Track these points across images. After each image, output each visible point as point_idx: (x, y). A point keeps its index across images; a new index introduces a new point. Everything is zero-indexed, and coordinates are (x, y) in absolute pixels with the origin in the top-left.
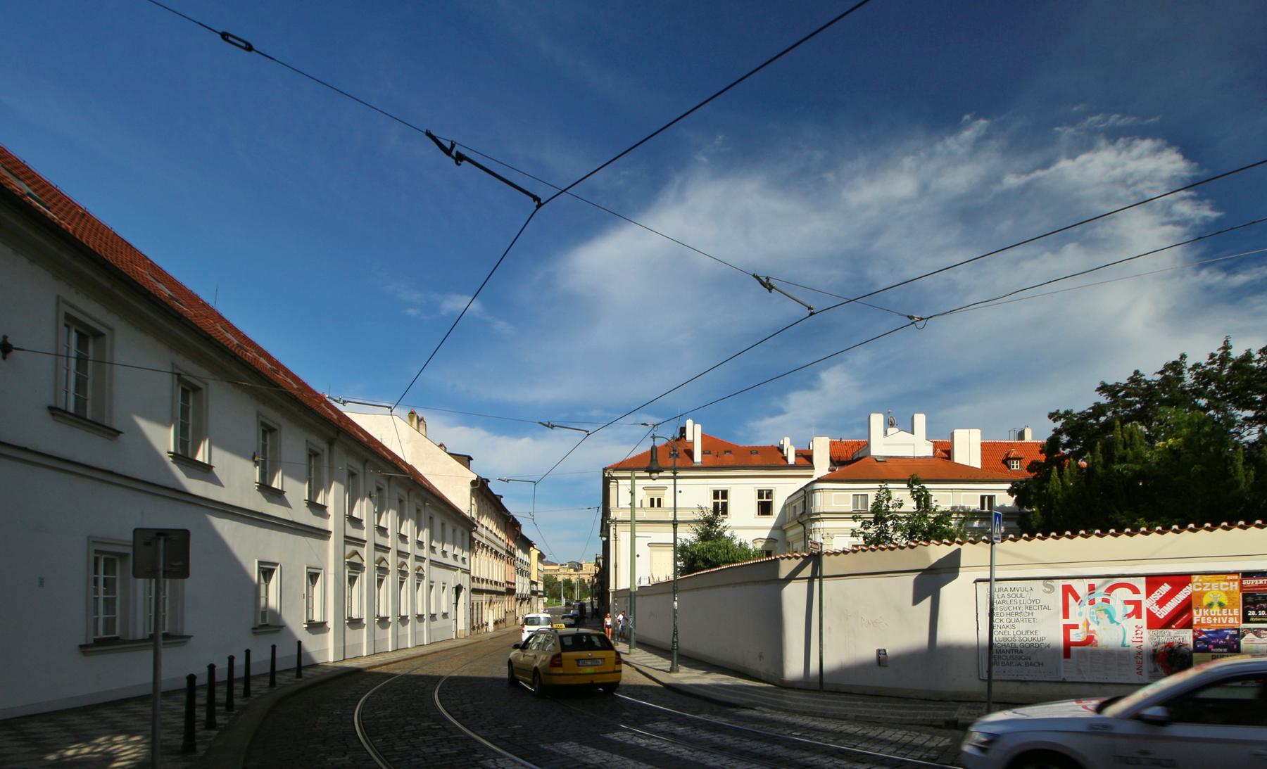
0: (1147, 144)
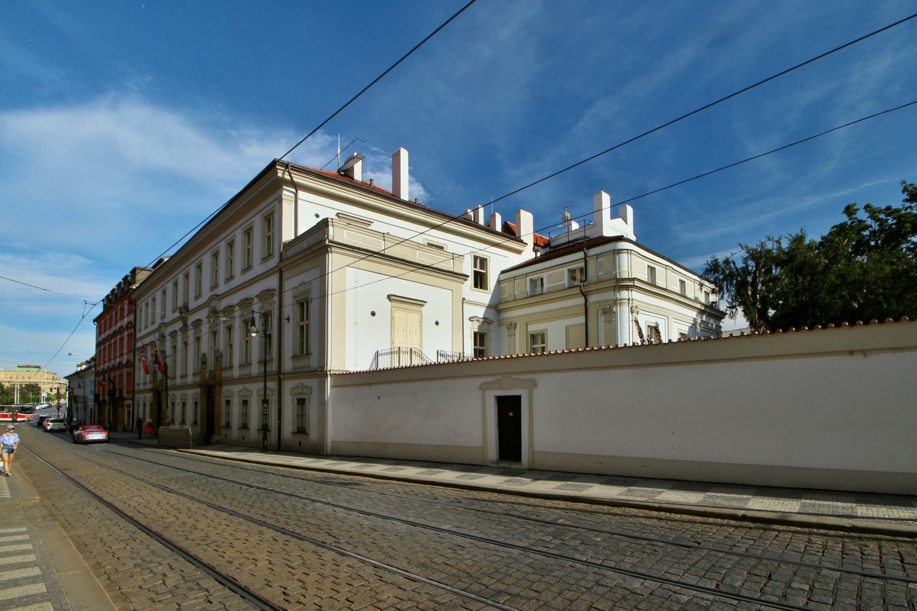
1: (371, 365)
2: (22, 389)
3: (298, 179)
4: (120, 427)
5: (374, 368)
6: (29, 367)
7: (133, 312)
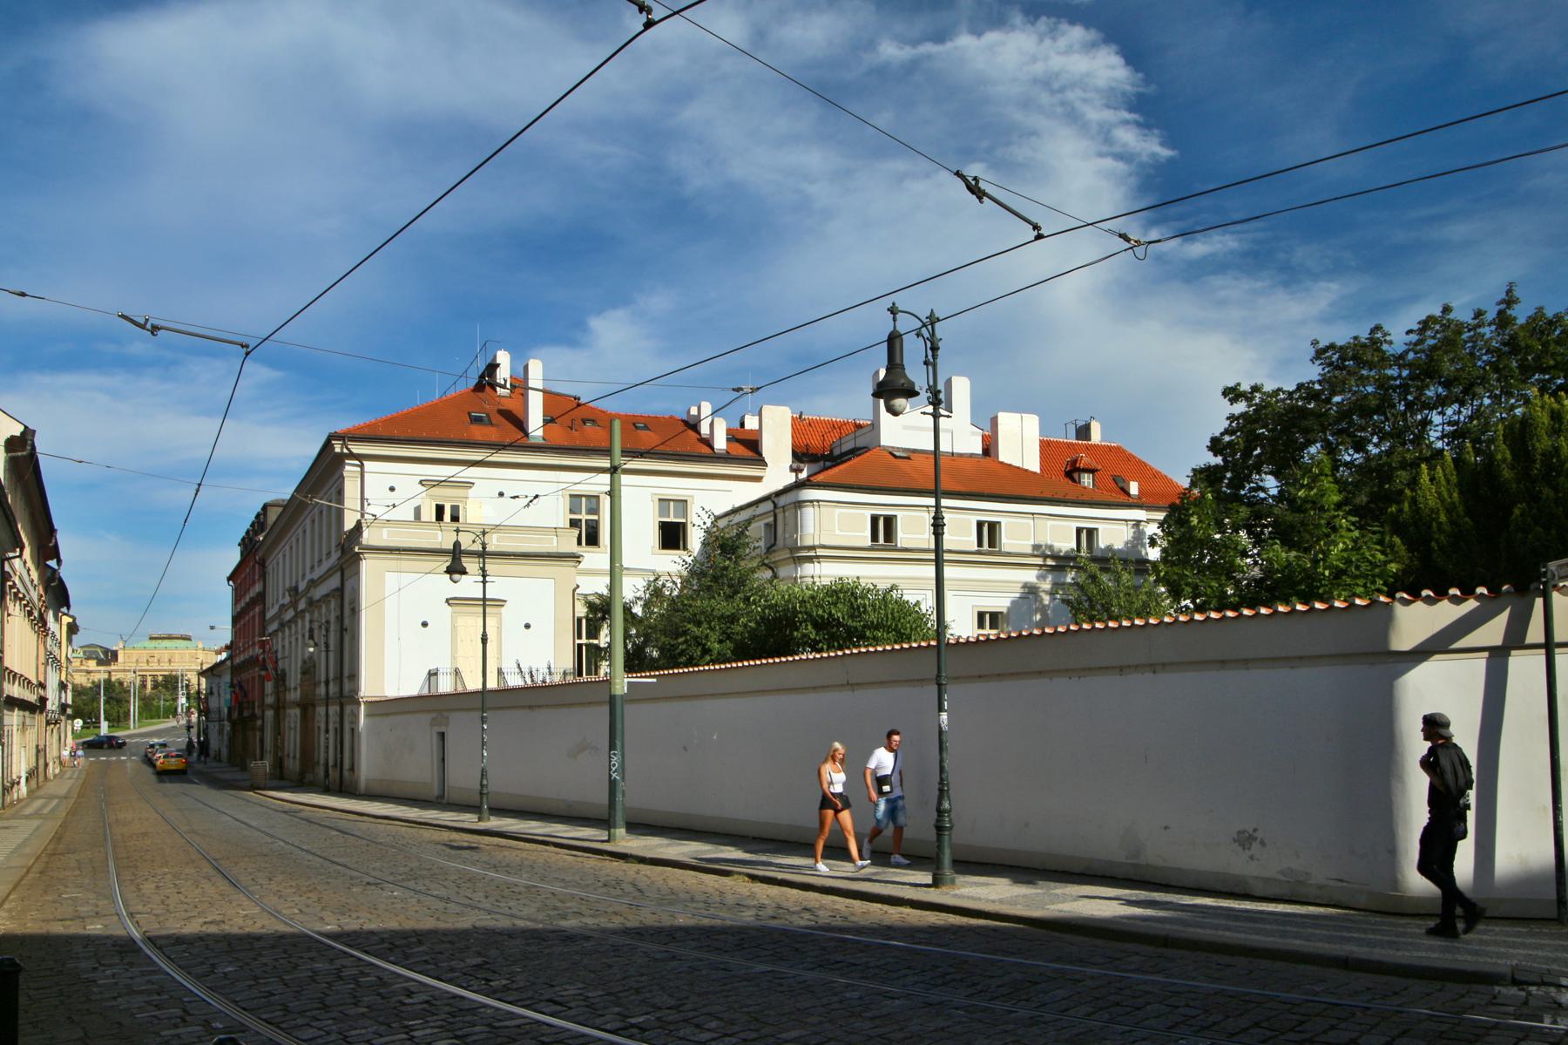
0: (1077, 33)
3: (357, 449)
5: (425, 692)
6: (170, 638)
7: (263, 576)
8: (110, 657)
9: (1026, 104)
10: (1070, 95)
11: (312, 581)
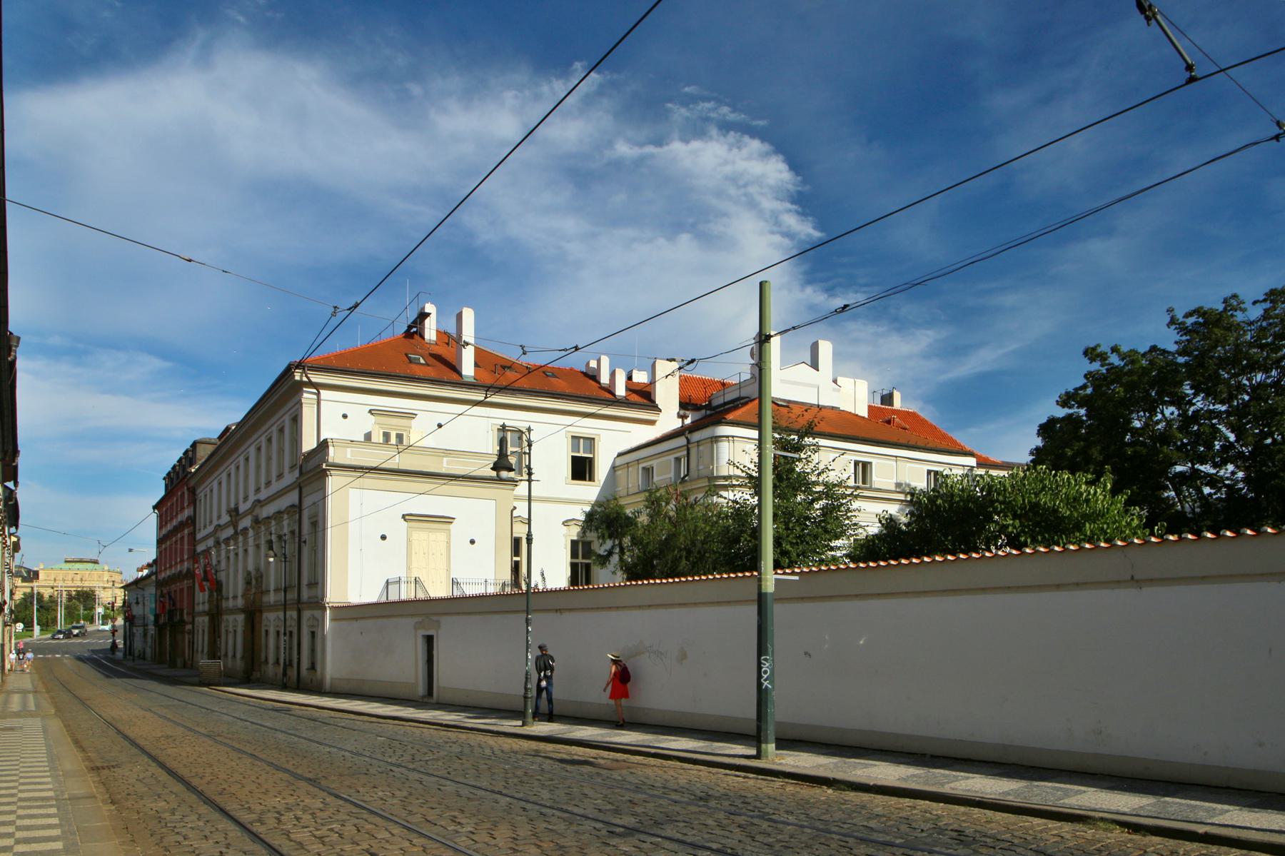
0: (755, 145)
1: (381, 595)
2: (70, 598)
3: (316, 378)
4: (179, 662)
5: (384, 599)
6: (81, 561)
7: (193, 502)
8: (32, 576)
9: (720, 194)
10: (751, 190)
11: (259, 501)
